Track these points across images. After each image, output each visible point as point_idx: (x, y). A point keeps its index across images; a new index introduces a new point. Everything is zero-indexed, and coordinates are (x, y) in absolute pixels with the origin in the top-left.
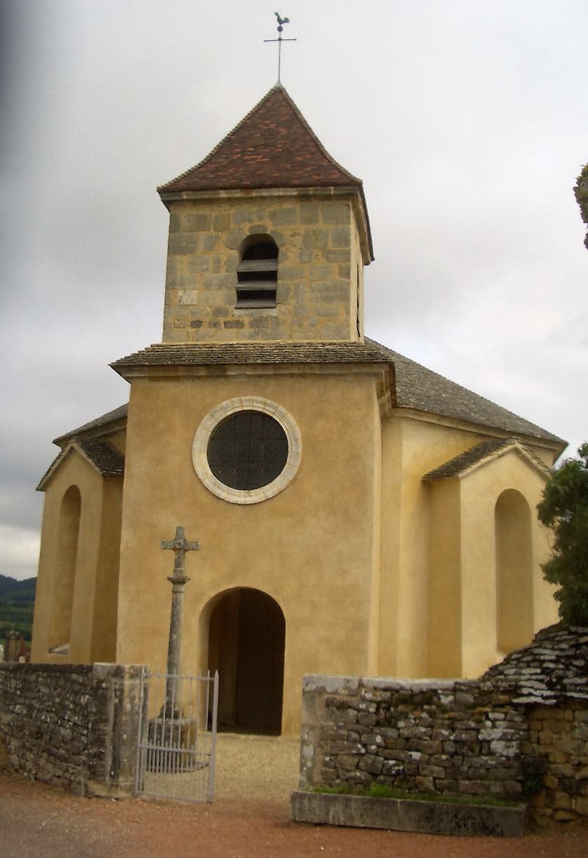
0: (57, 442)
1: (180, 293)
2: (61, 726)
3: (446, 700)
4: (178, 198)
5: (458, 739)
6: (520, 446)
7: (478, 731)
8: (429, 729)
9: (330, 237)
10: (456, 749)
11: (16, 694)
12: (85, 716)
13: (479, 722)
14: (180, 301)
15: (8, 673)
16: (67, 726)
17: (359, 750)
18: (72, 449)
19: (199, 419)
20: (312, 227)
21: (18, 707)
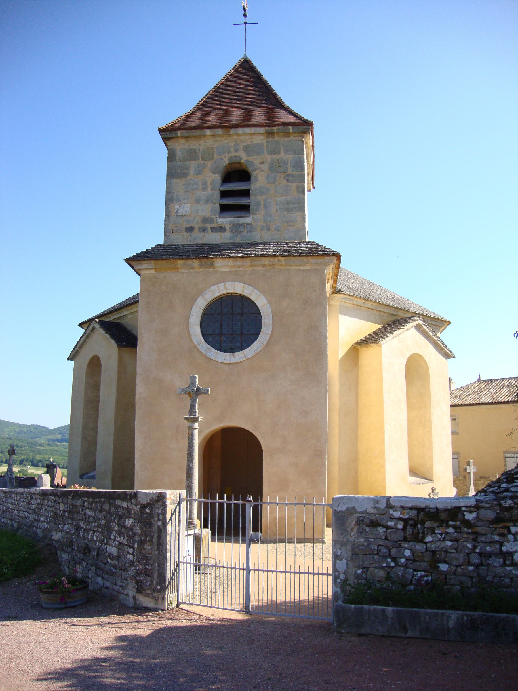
0: (81, 325)
1: (177, 207)
2: (106, 544)
3: (470, 517)
4: (173, 136)
5: (483, 551)
6: (421, 322)
7: (501, 544)
8: (455, 543)
9: (289, 164)
10: (481, 560)
11: (64, 516)
12: (131, 537)
13: (502, 535)
14: (177, 212)
15: (57, 498)
16: (113, 545)
17: (388, 563)
18: (94, 329)
19: (193, 300)
20: (276, 157)
21: (66, 526)
